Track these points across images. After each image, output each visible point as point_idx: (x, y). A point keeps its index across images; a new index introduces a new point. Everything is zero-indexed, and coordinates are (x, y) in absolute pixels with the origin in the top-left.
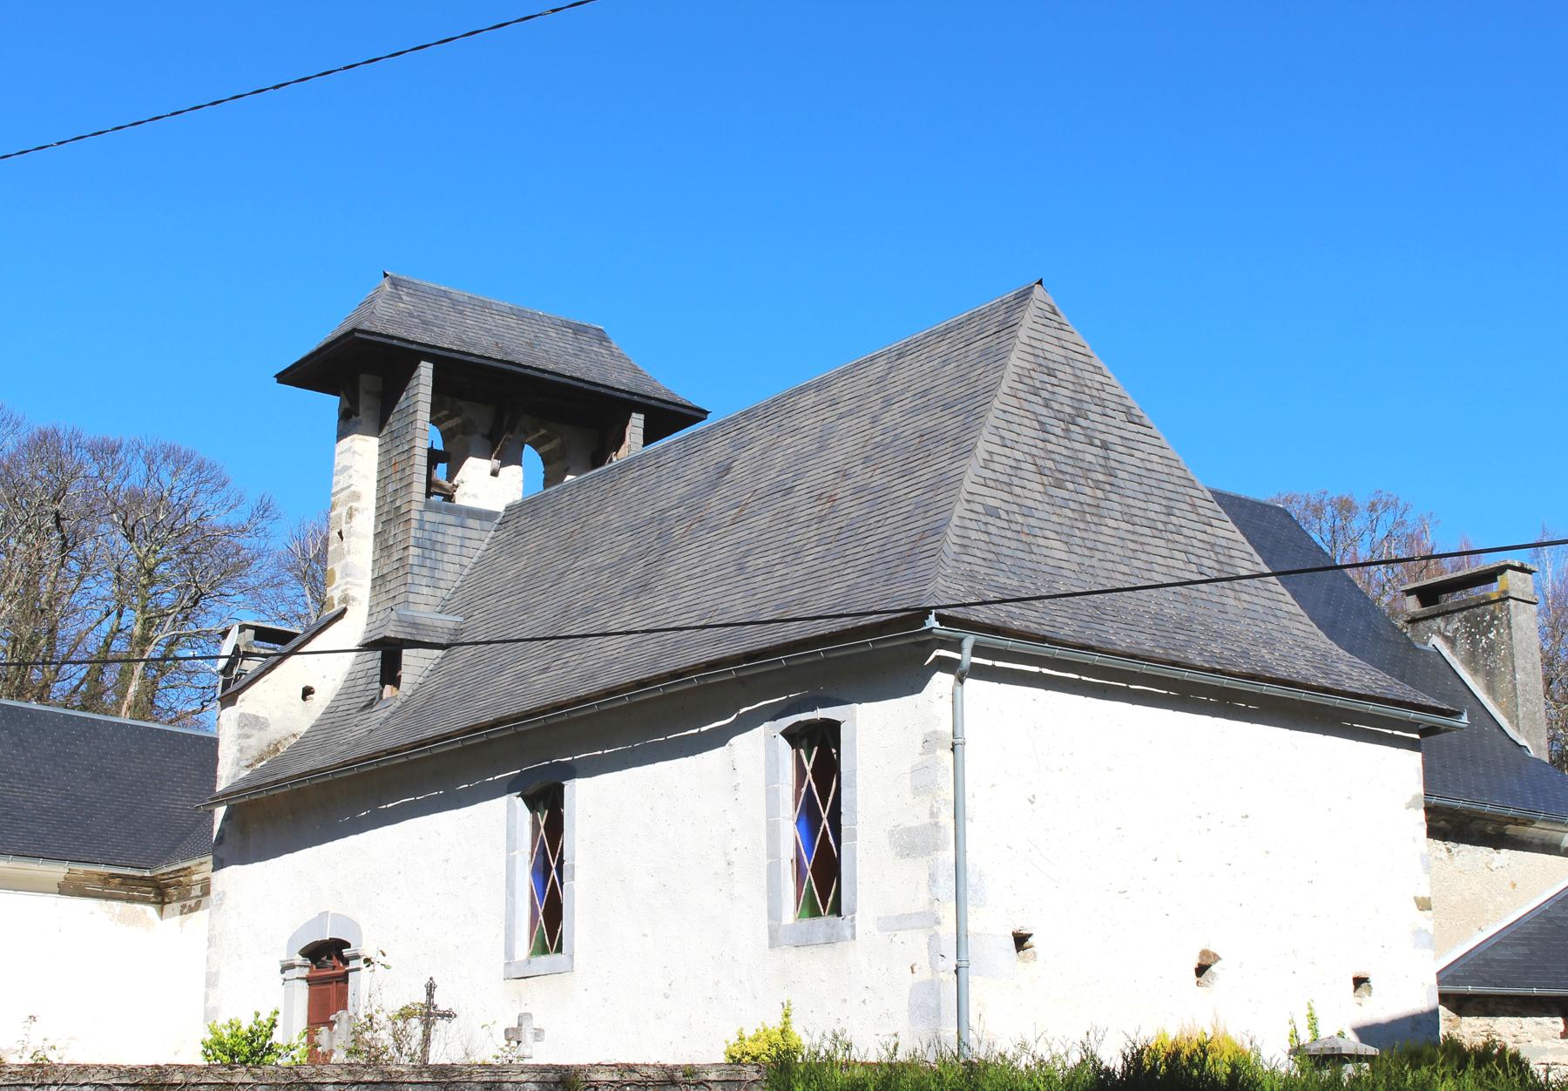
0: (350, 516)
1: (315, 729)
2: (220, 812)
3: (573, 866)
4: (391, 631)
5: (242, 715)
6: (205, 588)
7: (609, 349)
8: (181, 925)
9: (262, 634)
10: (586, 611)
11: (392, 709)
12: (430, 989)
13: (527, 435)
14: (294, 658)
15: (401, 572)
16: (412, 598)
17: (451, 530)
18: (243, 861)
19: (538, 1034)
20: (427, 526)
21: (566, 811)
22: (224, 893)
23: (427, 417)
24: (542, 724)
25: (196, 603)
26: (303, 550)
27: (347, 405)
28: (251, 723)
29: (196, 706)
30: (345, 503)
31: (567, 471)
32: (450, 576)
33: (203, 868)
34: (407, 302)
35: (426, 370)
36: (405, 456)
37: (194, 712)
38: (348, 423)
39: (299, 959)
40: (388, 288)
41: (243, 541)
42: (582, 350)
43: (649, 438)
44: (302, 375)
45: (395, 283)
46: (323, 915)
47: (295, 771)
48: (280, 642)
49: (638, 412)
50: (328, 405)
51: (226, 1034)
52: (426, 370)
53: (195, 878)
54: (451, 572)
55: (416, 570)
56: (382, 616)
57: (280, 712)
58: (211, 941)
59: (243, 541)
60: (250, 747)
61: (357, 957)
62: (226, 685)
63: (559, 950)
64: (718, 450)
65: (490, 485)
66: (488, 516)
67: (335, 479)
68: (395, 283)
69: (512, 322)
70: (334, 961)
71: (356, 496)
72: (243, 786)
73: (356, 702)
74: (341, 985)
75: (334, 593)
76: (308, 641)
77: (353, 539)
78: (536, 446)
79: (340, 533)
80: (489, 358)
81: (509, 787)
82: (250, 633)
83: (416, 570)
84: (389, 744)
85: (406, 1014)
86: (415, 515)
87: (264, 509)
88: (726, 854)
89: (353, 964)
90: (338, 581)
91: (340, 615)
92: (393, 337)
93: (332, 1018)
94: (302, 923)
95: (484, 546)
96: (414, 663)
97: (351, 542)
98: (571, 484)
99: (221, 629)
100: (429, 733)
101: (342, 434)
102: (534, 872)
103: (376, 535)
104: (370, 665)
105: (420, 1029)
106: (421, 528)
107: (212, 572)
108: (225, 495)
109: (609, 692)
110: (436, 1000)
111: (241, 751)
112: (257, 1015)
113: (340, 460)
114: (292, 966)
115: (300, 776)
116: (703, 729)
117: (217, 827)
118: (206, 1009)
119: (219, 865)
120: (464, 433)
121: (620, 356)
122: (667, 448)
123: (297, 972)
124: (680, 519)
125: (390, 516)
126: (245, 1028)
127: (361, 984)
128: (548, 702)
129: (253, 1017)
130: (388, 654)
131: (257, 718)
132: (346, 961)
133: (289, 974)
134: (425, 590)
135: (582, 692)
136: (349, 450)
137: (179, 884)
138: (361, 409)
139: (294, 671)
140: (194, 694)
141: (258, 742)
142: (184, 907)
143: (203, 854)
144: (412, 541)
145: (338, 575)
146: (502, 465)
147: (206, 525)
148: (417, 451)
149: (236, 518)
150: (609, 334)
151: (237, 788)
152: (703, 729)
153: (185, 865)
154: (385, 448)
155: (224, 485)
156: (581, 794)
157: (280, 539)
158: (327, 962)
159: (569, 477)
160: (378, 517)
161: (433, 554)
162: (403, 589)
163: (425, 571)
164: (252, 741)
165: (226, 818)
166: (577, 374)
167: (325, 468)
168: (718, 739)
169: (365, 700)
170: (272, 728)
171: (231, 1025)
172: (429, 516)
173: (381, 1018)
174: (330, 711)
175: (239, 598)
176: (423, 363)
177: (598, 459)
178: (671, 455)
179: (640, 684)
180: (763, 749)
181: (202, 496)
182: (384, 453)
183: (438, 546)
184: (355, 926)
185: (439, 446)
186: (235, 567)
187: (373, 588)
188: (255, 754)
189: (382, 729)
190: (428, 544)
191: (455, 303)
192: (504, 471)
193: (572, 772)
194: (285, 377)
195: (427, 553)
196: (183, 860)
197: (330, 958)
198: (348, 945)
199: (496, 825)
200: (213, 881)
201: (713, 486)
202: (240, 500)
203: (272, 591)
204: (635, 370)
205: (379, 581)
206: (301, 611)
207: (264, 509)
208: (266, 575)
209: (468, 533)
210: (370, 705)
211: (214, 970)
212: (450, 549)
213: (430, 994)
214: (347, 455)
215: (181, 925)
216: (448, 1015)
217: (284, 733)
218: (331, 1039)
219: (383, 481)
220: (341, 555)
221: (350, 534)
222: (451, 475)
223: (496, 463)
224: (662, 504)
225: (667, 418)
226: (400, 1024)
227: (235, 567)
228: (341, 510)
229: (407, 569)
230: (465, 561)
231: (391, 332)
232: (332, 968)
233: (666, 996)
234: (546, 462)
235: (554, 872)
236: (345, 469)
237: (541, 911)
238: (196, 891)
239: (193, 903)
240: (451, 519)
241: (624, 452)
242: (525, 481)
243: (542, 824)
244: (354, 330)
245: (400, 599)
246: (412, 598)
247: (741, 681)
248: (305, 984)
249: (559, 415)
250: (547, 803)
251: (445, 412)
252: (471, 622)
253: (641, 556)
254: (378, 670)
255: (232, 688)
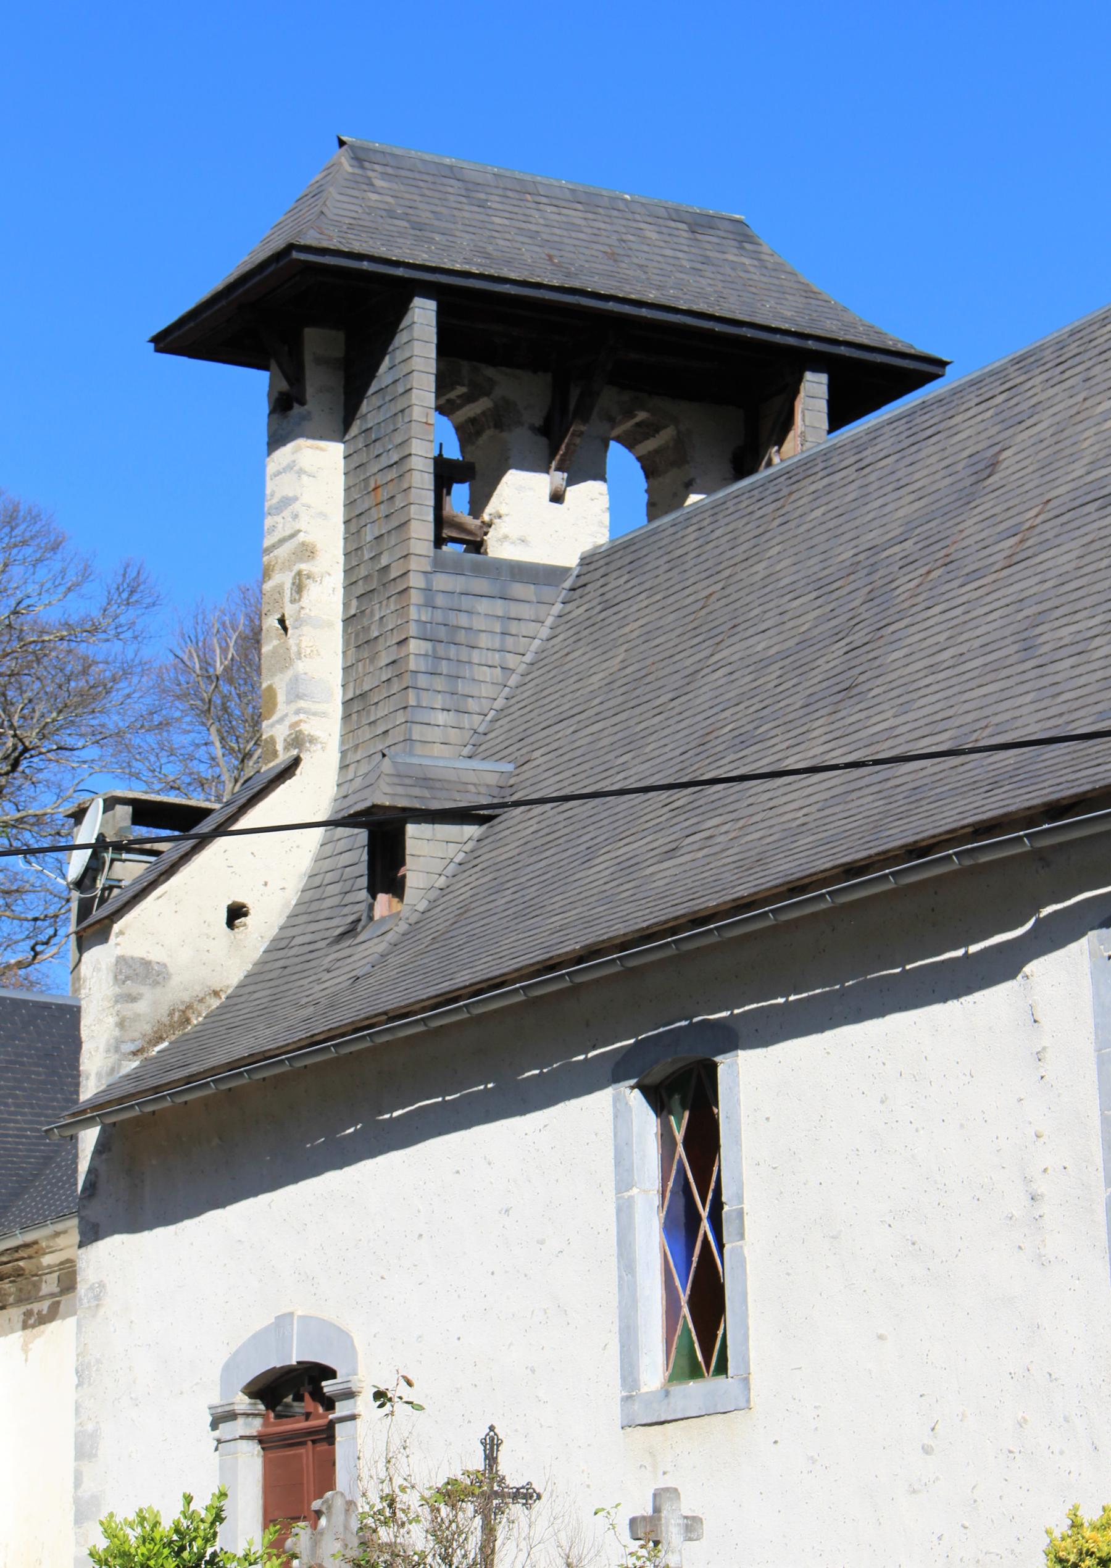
0: (299, 588)
1: (253, 979)
2: (89, 1138)
3: (740, 1214)
4: (386, 795)
5: (121, 960)
6: (31, 737)
7: (756, 255)
8: (25, 1348)
9: (145, 813)
10: (742, 741)
11: (390, 937)
12: (491, 1446)
13: (612, 422)
14: (222, 842)
15: (396, 687)
16: (417, 732)
17: (483, 606)
18: (135, 1225)
19: (692, 1526)
20: (440, 600)
21: (723, 1111)
22: (102, 1285)
23: (430, 399)
24: (672, 951)
25: (15, 765)
26: (206, 664)
27: (284, 386)
28: (138, 973)
29: (22, 953)
30: (287, 565)
31: (689, 487)
32: (486, 691)
33: (61, 1241)
34: (384, 189)
35: (423, 314)
36: (393, 474)
37: (20, 965)
38: (287, 416)
39: (243, 1402)
40: (347, 166)
41: (93, 648)
42: (707, 261)
43: (838, 417)
44: (207, 334)
45: (360, 157)
46: (284, 1320)
47: (221, 1057)
48: (178, 826)
49: (816, 370)
50: (252, 386)
51: (133, 1536)
52: (423, 314)
53: (47, 1260)
54: (487, 682)
55: (423, 681)
56: (364, 768)
57: (202, 940)
58: (82, 1375)
59: (93, 648)
60: (137, 1017)
61: (350, 1395)
62: (85, 910)
63: (722, 1368)
64: (971, 431)
65: (550, 519)
66: (548, 575)
67: (268, 522)
68: (360, 157)
69: (576, 216)
70: (309, 1404)
71: (307, 552)
72: (130, 1088)
73: (320, 927)
74: (323, 1447)
75: (276, 730)
76: (235, 817)
77: (305, 629)
78: (630, 443)
79: (282, 621)
80: (538, 286)
81: (617, 1071)
82: (124, 812)
83: (423, 681)
84: (391, 1000)
85: (452, 1494)
86: (416, 581)
87: (131, 589)
88: (1027, 1180)
89: (342, 1409)
90: (282, 708)
91: (289, 770)
92: (360, 257)
93: (316, 1505)
94: (246, 1336)
95: (545, 632)
96: (427, 850)
97: (302, 638)
98: (698, 508)
99: (70, 807)
100: (464, 978)
101: (276, 441)
102: (668, 1227)
103: (347, 621)
104: (347, 859)
105: (478, 1521)
106: (429, 604)
107: (41, 708)
108: (57, 566)
109: (795, 888)
110: (504, 1466)
111: (121, 1024)
112: (188, 1499)
113: (276, 487)
114: (231, 1416)
115: (231, 1066)
116: (973, 949)
117: (83, 1166)
118: (77, 1501)
119: (91, 1234)
120: (499, 425)
121: (779, 268)
122: (875, 434)
123: (240, 1427)
124: (908, 563)
125: (370, 585)
126: (166, 1526)
127: (366, 1446)
128: (681, 910)
129: (180, 1505)
130: (381, 838)
131: (146, 964)
132: (329, 1404)
133: (227, 1430)
134: (441, 718)
135: (744, 890)
136: (290, 467)
137: (19, 1273)
138: (310, 391)
139: (219, 869)
140: (19, 930)
141: (151, 1007)
142: (28, 1314)
143: (61, 1217)
144: (413, 629)
145: (281, 698)
146: (571, 482)
147: (25, 622)
148: (416, 463)
149: (81, 607)
150: (755, 229)
151: (117, 1094)
152: (973, 949)
153: (29, 1237)
154: (356, 460)
155: (55, 548)
156: (754, 1083)
157: (160, 641)
158: (295, 1402)
159: (693, 498)
160: (349, 586)
161: (453, 651)
162: (400, 717)
163: (439, 683)
164: (141, 1007)
165: (101, 1148)
166: (701, 306)
167: (250, 503)
168: (1004, 966)
169: (341, 924)
170: (175, 981)
171: (142, 1520)
172: (442, 582)
173: (410, 1500)
174: (279, 946)
175: (92, 752)
176: (418, 302)
177: (745, 461)
178: (886, 444)
179: (852, 870)
180: (1087, 981)
181: (16, 570)
182: (354, 469)
183: (461, 637)
184: (343, 1337)
185: (453, 452)
186: (83, 697)
187: (346, 717)
188: (147, 1028)
189: (393, 960)
190: (442, 633)
191: (470, 188)
192: (574, 493)
193: (731, 1038)
194: (170, 341)
195: (441, 649)
196: (24, 1228)
197: (299, 1398)
198: (330, 1373)
199: (590, 1147)
200: (81, 1265)
201: (967, 499)
202: (86, 574)
203: (151, 739)
204: (808, 293)
205: (356, 706)
206: (204, 771)
207: (131, 589)
208: (139, 706)
209: (515, 610)
210: (351, 931)
211: (90, 1427)
212: (484, 641)
213: (491, 1459)
214: (286, 478)
215: (25, 1348)
216: (526, 1496)
217: (198, 990)
218: (315, 1543)
219: (354, 521)
220: (285, 660)
221: (299, 622)
222: (477, 505)
223: (560, 477)
224: (873, 537)
225: (869, 379)
226: (445, 1511)
227: (83, 697)
228: (282, 579)
229: (407, 680)
230: (511, 661)
231: (357, 247)
232: (304, 1414)
233: (927, 1450)
234: (650, 471)
235: (705, 1226)
236: (286, 502)
237: (684, 1299)
238: (49, 1285)
239: (44, 1306)
240: (481, 585)
241: (792, 444)
242: (613, 509)
243: (679, 1136)
244: (291, 247)
245: (396, 736)
246: (417, 732)
247: (1040, 857)
248: (255, 1448)
249: (670, 382)
250: (688, 1098)
251: (461, 390)
252: (528, 772)
253: (837, 636)
254: (363, 868)
255: (97, 914)
